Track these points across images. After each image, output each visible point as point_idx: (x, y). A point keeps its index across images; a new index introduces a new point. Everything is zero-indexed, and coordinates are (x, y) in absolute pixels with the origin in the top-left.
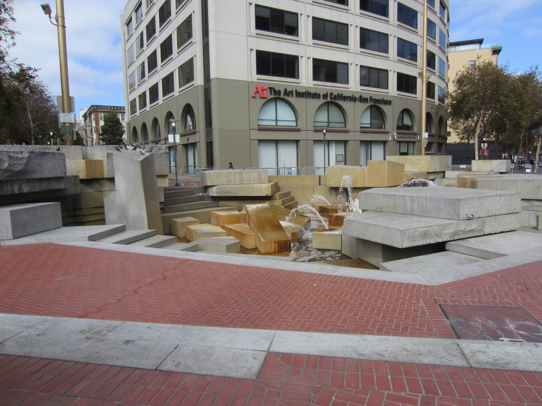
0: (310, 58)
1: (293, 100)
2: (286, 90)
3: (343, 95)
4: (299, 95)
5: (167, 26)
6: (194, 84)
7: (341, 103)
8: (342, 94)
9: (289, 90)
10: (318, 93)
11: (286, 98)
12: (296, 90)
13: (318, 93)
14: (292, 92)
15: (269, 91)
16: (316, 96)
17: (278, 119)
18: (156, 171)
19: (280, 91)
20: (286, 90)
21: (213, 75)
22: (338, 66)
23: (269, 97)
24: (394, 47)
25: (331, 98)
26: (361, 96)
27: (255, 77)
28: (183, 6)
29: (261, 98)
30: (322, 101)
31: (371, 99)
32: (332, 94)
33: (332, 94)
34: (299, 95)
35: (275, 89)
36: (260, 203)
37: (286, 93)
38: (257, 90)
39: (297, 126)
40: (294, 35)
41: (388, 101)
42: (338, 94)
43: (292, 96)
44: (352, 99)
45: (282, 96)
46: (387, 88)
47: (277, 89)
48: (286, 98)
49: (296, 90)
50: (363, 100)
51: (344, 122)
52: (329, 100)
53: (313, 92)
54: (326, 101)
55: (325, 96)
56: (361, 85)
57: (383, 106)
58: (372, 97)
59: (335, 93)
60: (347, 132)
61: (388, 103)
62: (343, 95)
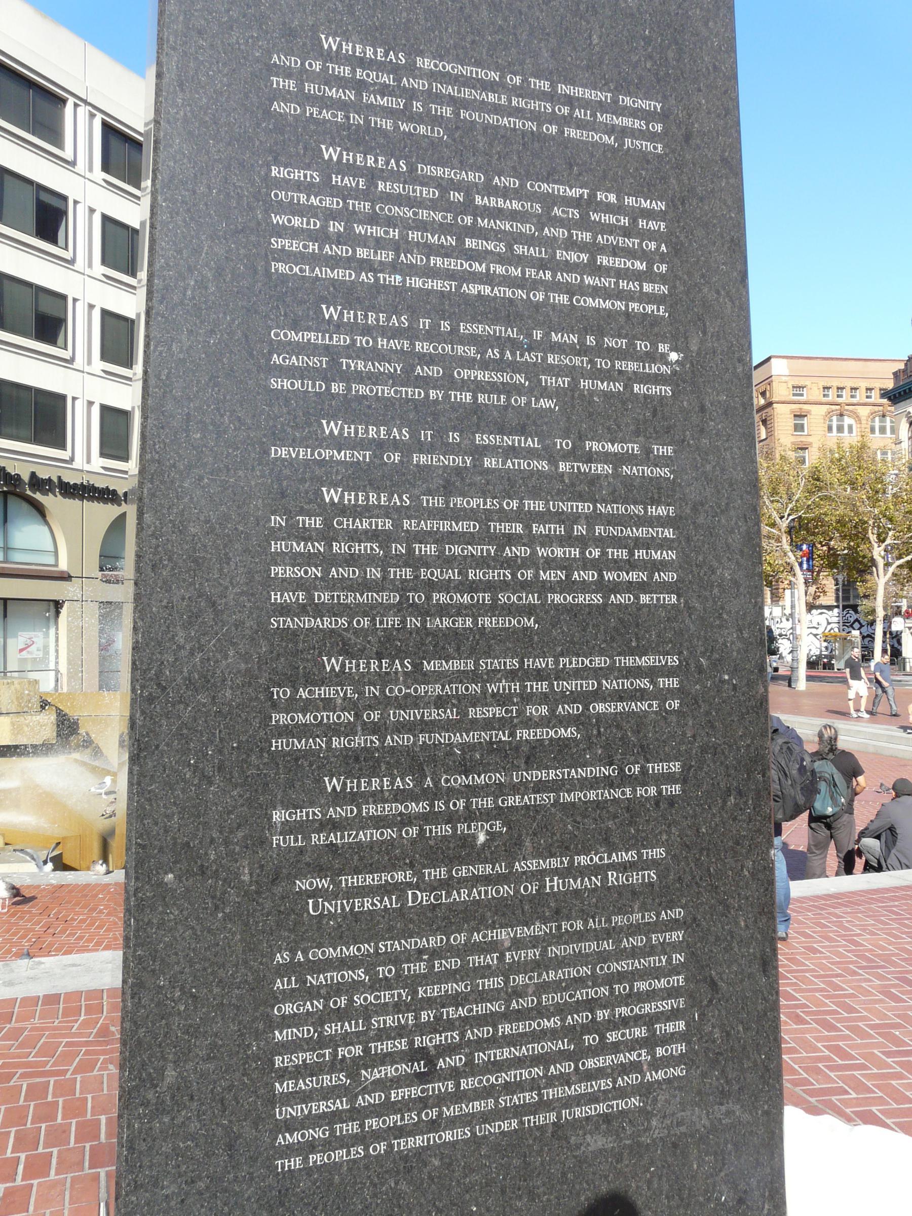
0: (93, 403)
1: (48, 501)
4: (70, 490)
9: (43, 474)
12: (59, 477)
20: (33, 475)
34: (70, 490)
39: (56, 565)
46: (60, 444)
51: (52, 549)
53: (100, 484)
56: (103, 454)
60: (65, 577)
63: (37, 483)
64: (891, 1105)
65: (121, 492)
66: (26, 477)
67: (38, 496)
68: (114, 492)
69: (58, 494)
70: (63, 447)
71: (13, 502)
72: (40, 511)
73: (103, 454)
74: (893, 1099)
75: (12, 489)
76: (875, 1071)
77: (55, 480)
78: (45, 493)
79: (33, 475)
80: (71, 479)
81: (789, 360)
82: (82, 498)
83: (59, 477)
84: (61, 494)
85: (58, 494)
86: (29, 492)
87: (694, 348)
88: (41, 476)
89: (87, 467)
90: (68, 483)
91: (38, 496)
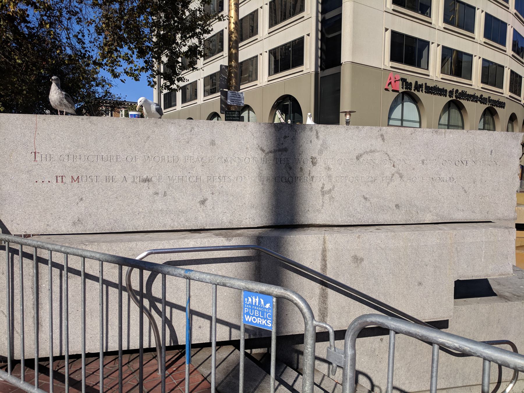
0: (440, 45)
1: (421, 95)
2: (416, 82)
3: (467, 93)
5: (177, 250)
6: (304, 69)
7: (464, 102)
8: (466, 92)
9: (419, 83)
10: (445, 89)
11: (416, 92)
13: (445, 89)
14: (421, 86)
15: (400, 82)
16: (441, 92)
17: (404, 119)
18: (286, 236)
19: (411, 83)
20: (416, 82)
21: (346, 56)
22: (464, 56)
23: (401, 90)
24: (510, 40)
25: (456, 96)
26: (482, 95)
27: (386, 63)
28: (263, 68)
29: (393, 91)
30: (448, 99)
31: (490, 100)
32: (457, 91)
33: (457, 91)
35: (407, 81)
36: (475, 346)
37: (418, 87)
40: (426, 15)
43: (422, 90)
44: (473, 98)
45: (413, 91)
47: (409, 81)
48: (416, 92)
49: (426, 84)
50: (482, 100)
52: (454, 98)
54: (451, 99)
55: (451, 92)
57: (498, 109)
58: (490, 97)
59: (460, 91)
61: (502, 105)
62: (467, 93)
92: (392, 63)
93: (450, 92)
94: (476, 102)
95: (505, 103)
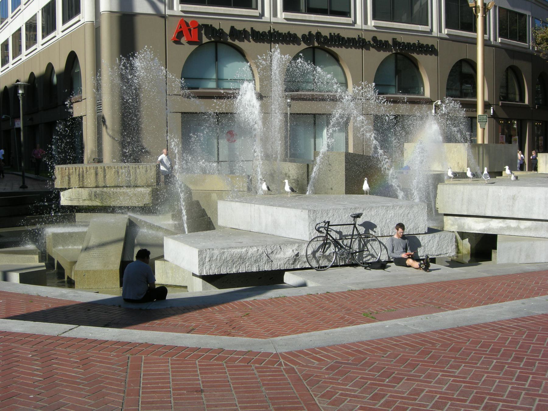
1: (244, 45)
9: (239, 27)
12: (252, 28)
20: (232, 28)
38: (181, 30)
41: (427, 45)
42: (330, 34)
50: (380, 45)
53: (283, 30)
56: (447, 26)
61: (430, 50)
63: (235, 33)
64: (329, 389)
65: (300, 36)
66: (227, 31)
67: (237, 43)
68: (295, 36)
69: (251, 40)
70: (427, 24)
71: (222, 49)
72: (336, 58)
73: (374, 17)
74: (330, 391)
75: (218, 39)
76: (357, 379)
77: (249, 31)
78: (241, 40)
79: (232, 28)
80: (260, 28)
81: (517, 221)
82: (270, 42)
83: (252, 28)
84: (254, 40)
85: (251, 40)
86: (230, 40)
87: (240, 314)
88: (238, 29)
89: (273, 20)
90: (259, 32)
91: (237, 43)
92: (182, 7)
93: (304, 36)
94: (368, 49)
95: (433, 46)
